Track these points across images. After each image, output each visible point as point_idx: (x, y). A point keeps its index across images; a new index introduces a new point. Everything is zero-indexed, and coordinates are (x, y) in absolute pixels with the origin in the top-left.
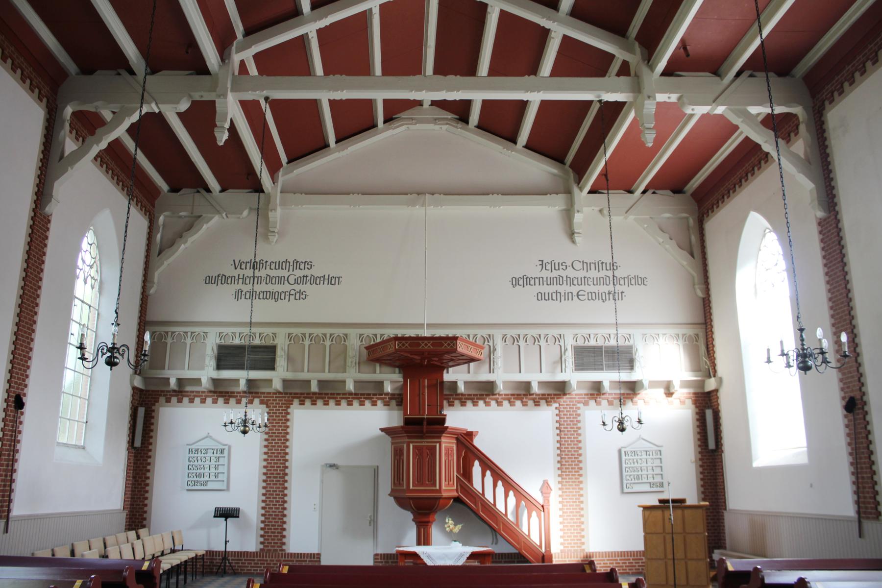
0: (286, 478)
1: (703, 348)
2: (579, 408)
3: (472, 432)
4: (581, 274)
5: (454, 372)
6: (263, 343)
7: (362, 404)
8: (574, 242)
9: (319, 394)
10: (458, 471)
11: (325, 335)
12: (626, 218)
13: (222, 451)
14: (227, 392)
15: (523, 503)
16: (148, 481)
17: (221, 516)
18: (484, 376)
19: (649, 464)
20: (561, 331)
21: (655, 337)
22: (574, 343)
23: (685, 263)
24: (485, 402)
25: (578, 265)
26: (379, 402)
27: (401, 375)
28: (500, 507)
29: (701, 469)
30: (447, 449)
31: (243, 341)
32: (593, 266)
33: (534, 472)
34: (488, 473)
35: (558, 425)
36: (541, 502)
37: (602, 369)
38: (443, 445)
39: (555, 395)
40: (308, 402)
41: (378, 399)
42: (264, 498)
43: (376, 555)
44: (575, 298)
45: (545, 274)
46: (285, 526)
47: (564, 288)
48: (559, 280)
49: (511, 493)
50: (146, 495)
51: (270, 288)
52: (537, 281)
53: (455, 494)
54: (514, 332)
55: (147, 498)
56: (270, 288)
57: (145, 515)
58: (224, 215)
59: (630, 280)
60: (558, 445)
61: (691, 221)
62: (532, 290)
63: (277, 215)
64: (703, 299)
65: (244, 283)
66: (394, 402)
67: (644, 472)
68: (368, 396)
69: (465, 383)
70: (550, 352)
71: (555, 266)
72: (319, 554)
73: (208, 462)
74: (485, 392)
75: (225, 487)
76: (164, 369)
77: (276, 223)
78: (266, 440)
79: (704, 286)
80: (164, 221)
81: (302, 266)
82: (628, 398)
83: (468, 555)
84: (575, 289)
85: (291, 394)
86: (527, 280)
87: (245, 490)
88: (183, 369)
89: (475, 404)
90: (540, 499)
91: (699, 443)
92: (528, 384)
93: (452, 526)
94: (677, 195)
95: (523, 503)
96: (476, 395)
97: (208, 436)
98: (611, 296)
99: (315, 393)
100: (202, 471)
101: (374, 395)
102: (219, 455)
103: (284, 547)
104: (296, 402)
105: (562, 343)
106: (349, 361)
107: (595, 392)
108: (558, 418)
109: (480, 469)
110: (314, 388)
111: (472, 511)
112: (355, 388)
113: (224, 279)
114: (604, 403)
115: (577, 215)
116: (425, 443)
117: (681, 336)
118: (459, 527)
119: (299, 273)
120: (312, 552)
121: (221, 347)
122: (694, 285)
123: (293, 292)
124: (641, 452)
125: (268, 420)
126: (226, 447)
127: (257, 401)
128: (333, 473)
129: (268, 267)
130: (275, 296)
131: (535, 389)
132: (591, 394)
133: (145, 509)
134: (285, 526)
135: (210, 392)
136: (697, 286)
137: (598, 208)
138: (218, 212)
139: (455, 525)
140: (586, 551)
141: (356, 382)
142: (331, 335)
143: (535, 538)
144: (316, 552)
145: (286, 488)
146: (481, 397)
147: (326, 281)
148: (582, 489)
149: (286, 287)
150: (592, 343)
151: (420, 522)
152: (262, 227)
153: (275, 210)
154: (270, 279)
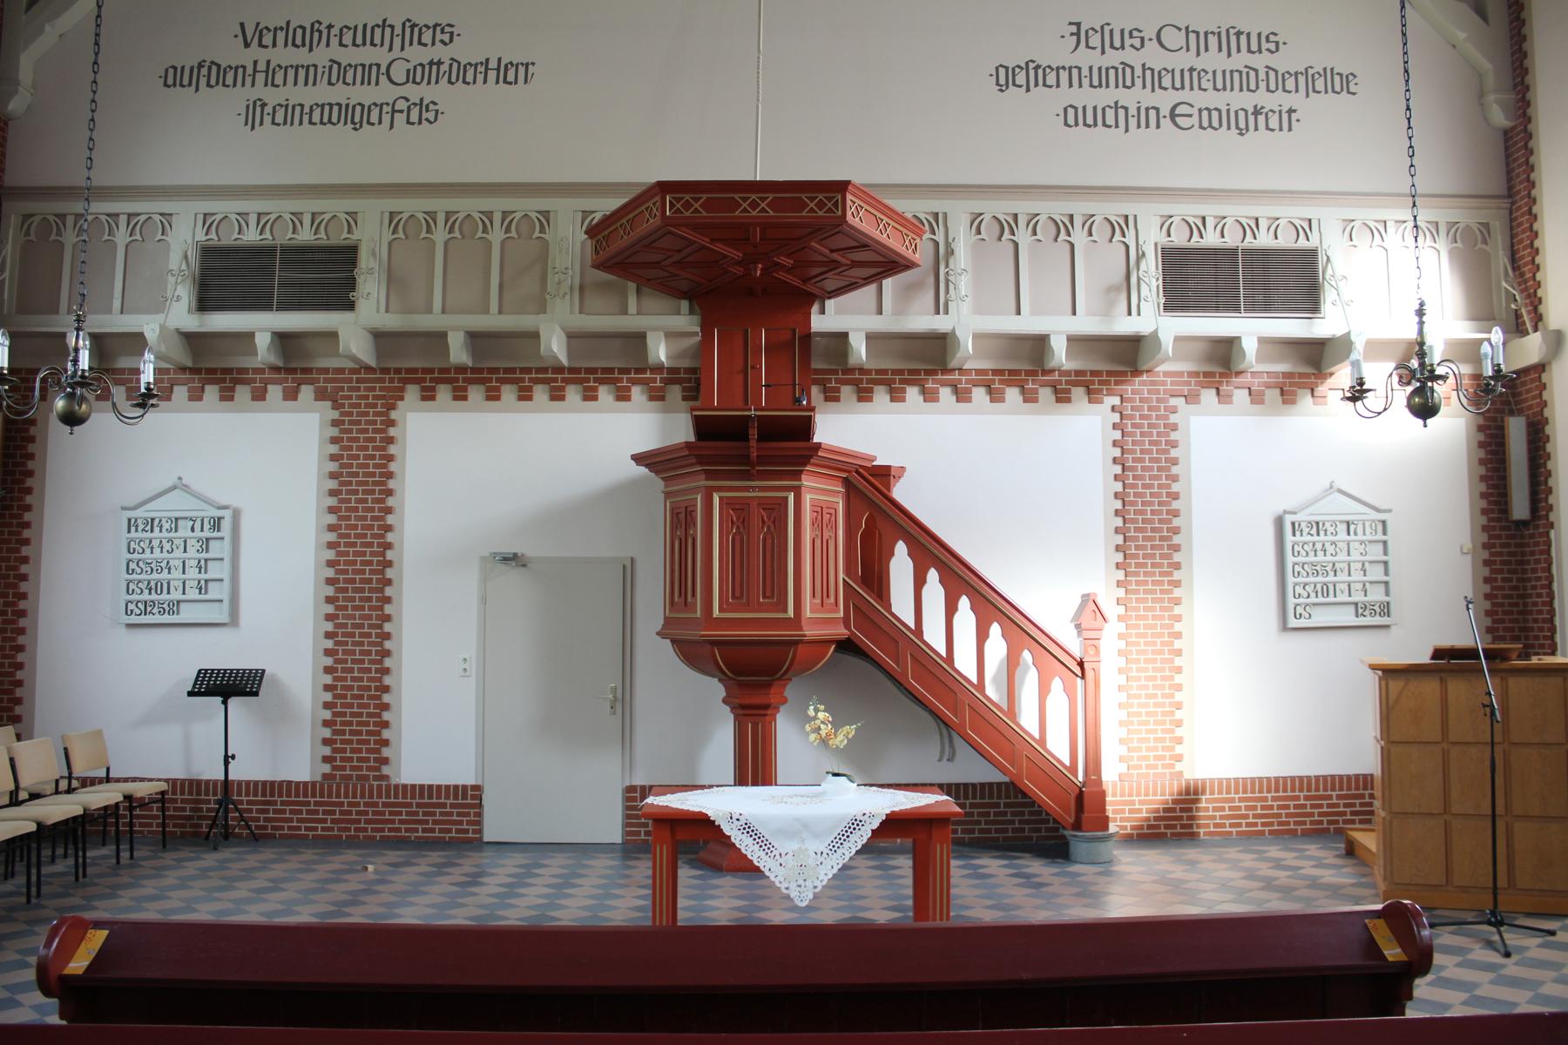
0: (388, 591)
1: (1501, 260)
2: (1174, 410)
3: (889, 467)
4: (1184, 60)
9: (474, 370)
10: (849, 570)
11: (489, 214)
13: (217, 524)
14: (228, 371)
15: (1027, 656)
16: (22, 605)
18: (921, 321)
19: (1355, 556)
21: (1377, 230)
22: (1163, 240)
24: (924, 392)
25: (1173, 38)
27: (696, 319)
28: (965, 663)
29: (1486, 572)
30: (819, 510)
32: (1213, 40)
33: (1055, 572)
35: (1117, 452)
36: (1077, 654)
37: (1237, 309)
38: (807, 498)
39: (1110, 373)
41: (635, 382)
42: (329, 644)
45: (1086, 58)
46: (386, 716)
47: (1134, 97)
48: (1122, 76)
50: (21, 640)
51: (340, 94)
52: (1064, 75)
53: (841, 632)
55: (21, 648)
56: (340, 94)
60: (1118, 505)
64: (1507, 134)
66: (675, 392)
67: (1342, 577)
68: (607, 376)
69: (870, 337)
70: (1098, 262)
71: (1111, 39)
72: (477, 788)
73: (178, 553)
74: (922, 364)
75: (224, 618)
76: (57, 312)
81: (427, 38)
82: (1302, 386)
83: (875, 825)
85: (398, 371)
86: (1035, 74)
87: (278, 617)
88: (109, 311)
89: (897, 396)
90: (1074, 644)
92: (1040, 343)
95: (1027, 656)
96: (901, 372)
97: (179, 486)
98: (1261, 118)
99: (461, 369)
100: (165, 575)
101: (623, 371)
103: (385, 770)
104: (412, 392)
107: (1218, 370)
109: (910, 564)
110: (458, 353)
111: (885, 672)
113: (215, 74)
114: (1241, 396)
116: (756, 490)
118: (850, 730)
119: (418, 55)
126: (227, 514)
127: (307, 392)
128: (513, 575)
129: (334, 41)
132: (1206, 374)
134: (386, 716)
135: (183, 369)
139: (837, 725)
140: (1188, 775)
143: (1058, 746)
144: (471, 781)
145: (388, 618)
146: (914, 377)
147: (492, 75)
148: (1178, 618)
149: (384, 92)
150: (1211, 239)
151: (743, 707)
154: (339, 72)
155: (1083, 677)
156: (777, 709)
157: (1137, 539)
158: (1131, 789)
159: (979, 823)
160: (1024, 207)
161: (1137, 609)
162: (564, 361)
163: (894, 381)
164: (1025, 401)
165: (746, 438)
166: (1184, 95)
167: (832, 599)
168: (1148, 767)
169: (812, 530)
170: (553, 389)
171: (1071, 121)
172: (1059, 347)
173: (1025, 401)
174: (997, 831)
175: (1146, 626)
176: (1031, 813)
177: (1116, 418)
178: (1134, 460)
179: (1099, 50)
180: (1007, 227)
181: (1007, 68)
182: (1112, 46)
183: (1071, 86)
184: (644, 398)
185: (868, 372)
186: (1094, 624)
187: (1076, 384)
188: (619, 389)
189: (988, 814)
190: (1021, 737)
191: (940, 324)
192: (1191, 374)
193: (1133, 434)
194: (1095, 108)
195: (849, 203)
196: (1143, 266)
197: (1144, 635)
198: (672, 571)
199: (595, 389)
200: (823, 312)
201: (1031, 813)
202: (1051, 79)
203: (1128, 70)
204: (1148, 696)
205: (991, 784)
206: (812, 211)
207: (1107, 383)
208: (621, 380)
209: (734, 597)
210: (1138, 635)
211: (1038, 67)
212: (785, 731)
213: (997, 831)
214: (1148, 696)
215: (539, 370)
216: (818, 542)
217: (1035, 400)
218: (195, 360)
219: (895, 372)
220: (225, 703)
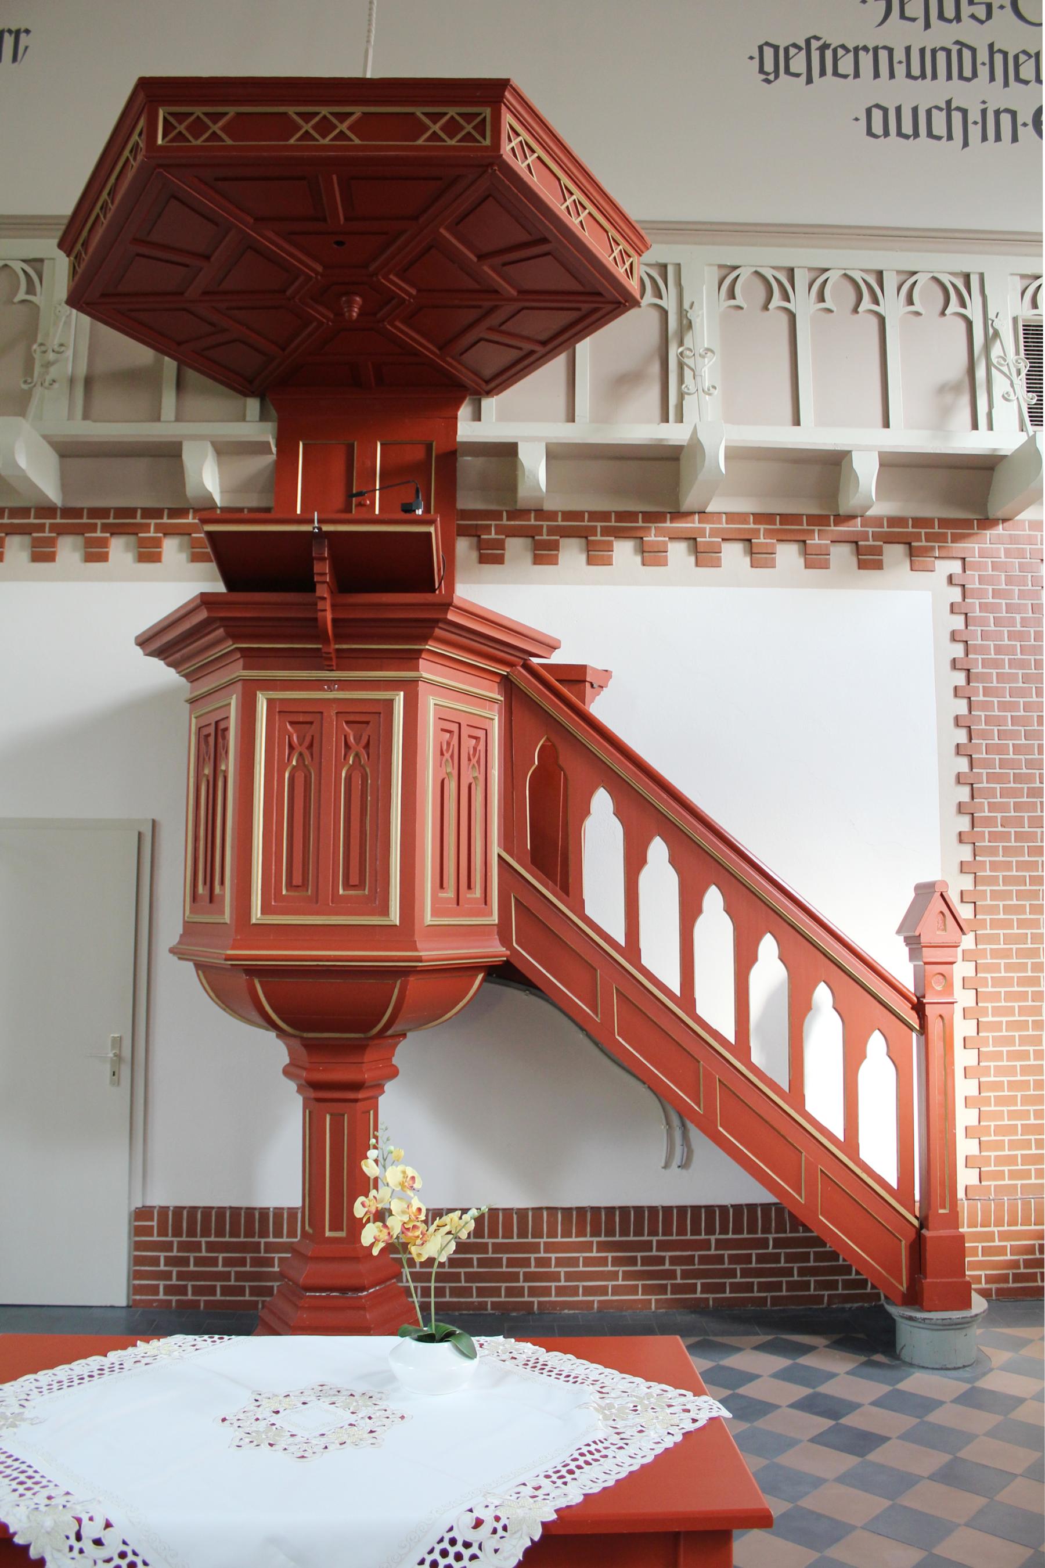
3: (583, 668)
5: (503, 416)
7: (95, 554)
10: (508, 840)
15: (822, 995)
18: (639, 427)
26: (170, 547)
28: (715, 1008)
30: (452, 728)
38: (430, 704)
39: (944, 523)
43: (142, 1213)
52: (866, 60)
53: (494, 950)
54: (769, 258)
62: (850, 95)
68: (123, 521)
70: (923, 351)
74: (639, 500)
86: (822, 58)
90: (901, 969)
92: (833, 465)
96: (605, 516)
112: (65, 487)
116: (332, 689)
143: (880, 1154)
146: (625, 524)
155: (923, 1029)
156: (380, 1088)
157: (991, 793)
158: (986, 1213)
159: (732, 1273)
160: (803, 257)
161: (993, 909)
162: (53, 494)
163: (593, 531)
164: (807, 566)
165: (308, 586)
167: (478, 893)
168: (1013, 1175)
169: (439, 765)
170: (36, 543)
171: (877, 128)
172: (866, 470)
173: (807, 566)
174: (762, 1287)
175: (1008, 939)
176: (818, 1257)
177: (955, 594)
178: (985, 663)
179: (921, 22)
180: (776, 287)
181: (776, 48)
182: (941, 16)
183: (877, 75)
184: (183, 557)
185: (552, 515)
186: (941, 937)
187: (891, 539)
188: (142, 543)
189: (748, 1259)
190: (811, 1134)
191: (674, 434)
193: (983, 622)
194: (915, 110)
195: (505, 129)
196: (996, 351)
197: (1006, 954)
198: (196, 839)
199: (104, 543)
200: (477, 416)
201: (818, 1257)
203: (967, 54)
204: (1013, 1056)
205: (752, 1207)
206: (435, 135)
207: (940, 538)
208: (146, 528)
209: (290, 885)
210: (995, 953)
211: (824, 47)
212: (1000, 514)
213: (762, 1287)
214: (1013, 1056)
215: (15, 512)
216: (451, 787)
217: (825, 565)
219: (594, 516)
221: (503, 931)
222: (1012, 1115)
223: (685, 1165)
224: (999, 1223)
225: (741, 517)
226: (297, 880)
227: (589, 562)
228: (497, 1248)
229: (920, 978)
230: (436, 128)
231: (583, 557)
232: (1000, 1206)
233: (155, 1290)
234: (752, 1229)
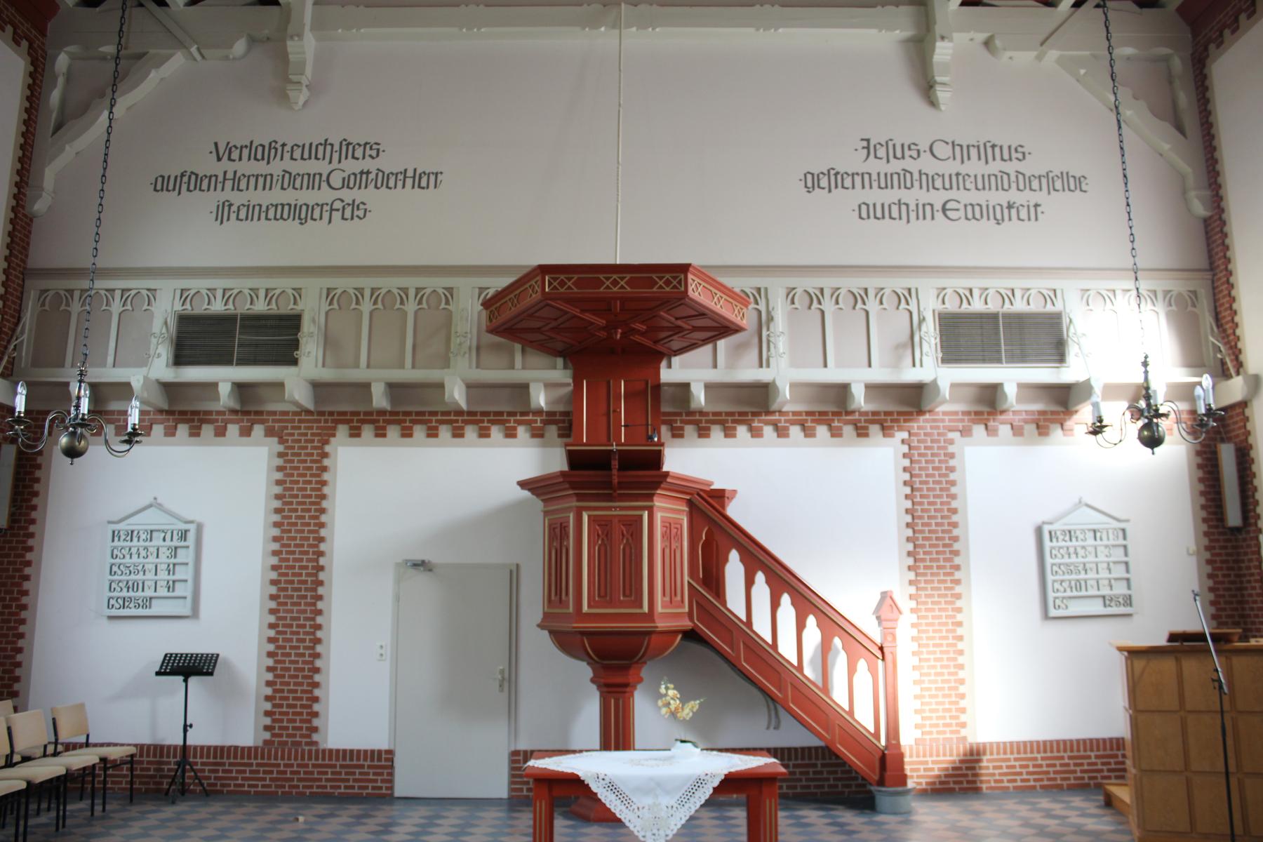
1: (1208, 319)
2: (951, 442)
3: (723, 491)
4: (951, 167)
5: (683, 366)
6: (274, 309)
8: (933, 103)
10: (693, 574)
12: (1039, 58)
13: (184, 535)
15: (837, 642)
17: (173, 672)
18: (748, 373)
19: (1102, 558)
20: (912, 282)
22: (940, 307)
23: (1166, 147)
24: (751, 429)
26: (521, 430)
27: (569, 372)
28: (787, 649)
29: (1209, 569)
30: (668, 525)
31: (230, 306)
32: (973, 152)
34: (760, 577)
35: (907, 476)
37: (999, 361)
38: (659, 516)
39: (899, 413)
40: (367, 431)
41: (520, 423)
42: (272, 633)
44: (939, 215)
45: (874, 166)
46: (317, 692)
47: (914, 196)
48: (903, 180)
49: (811, 621)
50: (22, 629)
51: (290, 196)
52: (858, 179)
53: (686, 624)
55: (22, 636)
56: (290, 196)
57: (18, 672)
58: (194, 49)
59: (1049, 181)
61: (1177, 64)
63: (305, 47)
64: (1206, 221)
65: (236, 187)
66: (552, 430)
67: (1091, 575)
68: (498, 418)
70: (887, 326)
71: (895, 151)
72: (390, 752)
73: (152, 559)
74: (750, 407)
75: (186, 611)
77: (302, 64)
78: (277, 511)
79: (1208, 193)
80: (70, 68)
81: (359, 153)
82: (1053, 421)
83: (716, 783)
84: (938, 198)
85: (331, 414)
87: (232, 620)
89: (729, 433)
91: (1204, 514)
92: (842, 391)
93: (674, 704)
94: (1145, 10)
96: (732, 414)
97: (155, 504)
99: (382, 412)
100: (140, 576)
101: (510, 414)
102: (176, 543)
103: (315, 737)
104: (342, 430)
105: (913, 306)
106: (455, 341)
108: (907, 462)
110: (380, 399)
112: (468, 401)
113: (192, 181)
114: (1005, 430)
115: (939, 44)
116: (616, 510)
117: (1160, 296)
118: (694, 705)
119: (351, 166)
120: (376, 747)
121: (185, 321)
122: (1184, 192)
123: (338, 205)
124: (1083, 531)
125: (140, 420)
126: (192, 527)
127: (258, 430)
130: (302, 214)
131: (859, 398)
132: (976, 413)
133: (19, 658)
135: (161, 411)
136: (1192, 194)
137: (981, 37)
138: (181, 45)
141: (470, 387)
142: (418, 290)
143: (864, 717)
146: (743, 418)
147: (409, 182)
149: (325, 195)
150: (977, 306)
151: (607, 685)
152: (282, 78)
153: (300, 36)
154: (290, 180)
155: (883, 659)
156: (634, 687)
163: (727, 421)
166: (953, 194)
167: (679, 598)
168: (938, 733)
170: (454, 429)
171: (864, 215)
172: (859, 393)
174: (816, 787)
176: (843, 772)
177: (905, 449)
179: (885, 160)
180: (814, 298)
184: (527, 435)
185: (706, 414)
187: (873, 422)
188: (507, 428)
191: (763, 375)
192: (964, 413)
196: (924, 328)
199: (488, 429)
200: (669, 366)
202: (848, 182)
203: (908, 175)
204: (937, 674)
206: (661, 286)
207: (897, 421)
212: (928, 408)
213: (816, 787)
215: (444, 413)
216: (667, 551)
218: (170, 405)
219: (728, 414)
220: (186, 681)
221: (690, 614)
222: (937, 703)
223: (777, 728)
224: (931, 755)
225: (799, 413)
226: (602, 593)
227: (726, 436)
228: (258, 765)
229: (884, 636)
230: (661, 283)
231: (722, 434)
232: (931, 747)
233: (521, 790)
234: (810, 758)
